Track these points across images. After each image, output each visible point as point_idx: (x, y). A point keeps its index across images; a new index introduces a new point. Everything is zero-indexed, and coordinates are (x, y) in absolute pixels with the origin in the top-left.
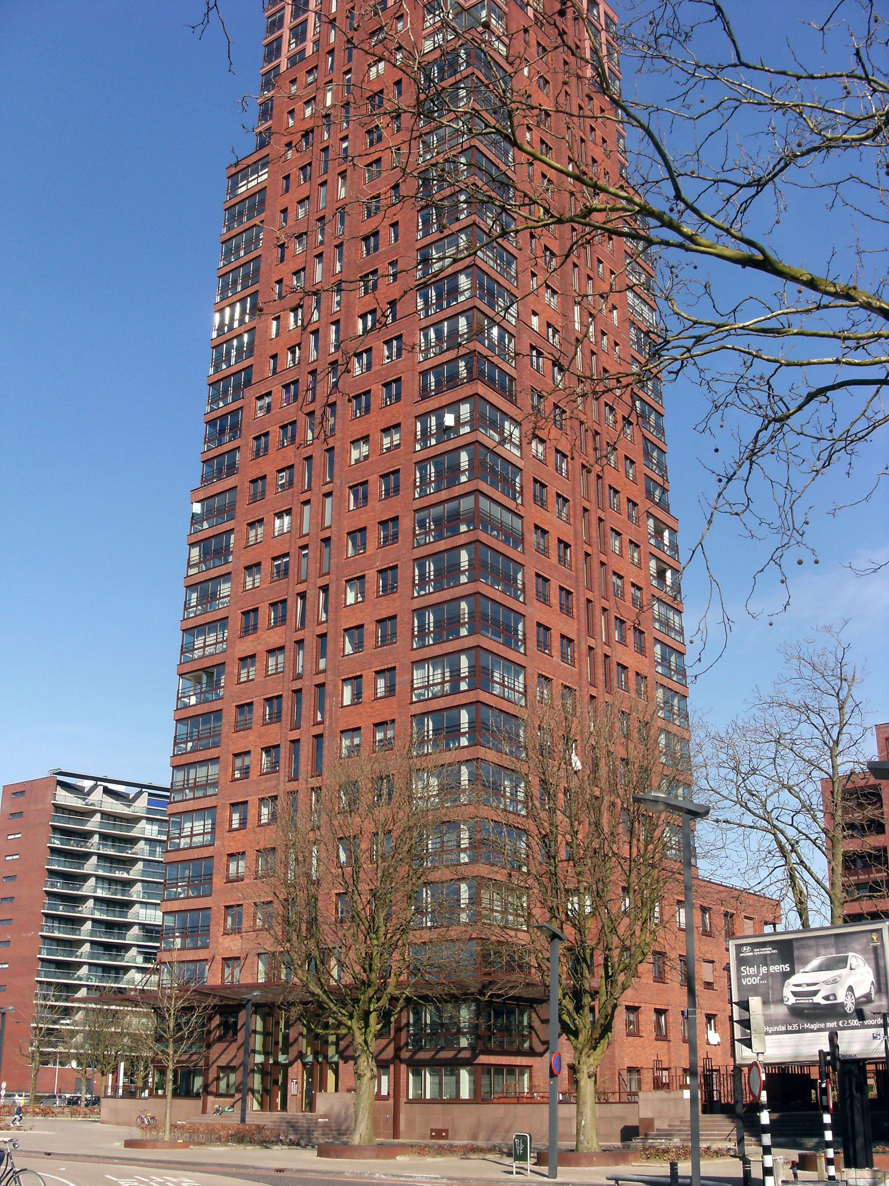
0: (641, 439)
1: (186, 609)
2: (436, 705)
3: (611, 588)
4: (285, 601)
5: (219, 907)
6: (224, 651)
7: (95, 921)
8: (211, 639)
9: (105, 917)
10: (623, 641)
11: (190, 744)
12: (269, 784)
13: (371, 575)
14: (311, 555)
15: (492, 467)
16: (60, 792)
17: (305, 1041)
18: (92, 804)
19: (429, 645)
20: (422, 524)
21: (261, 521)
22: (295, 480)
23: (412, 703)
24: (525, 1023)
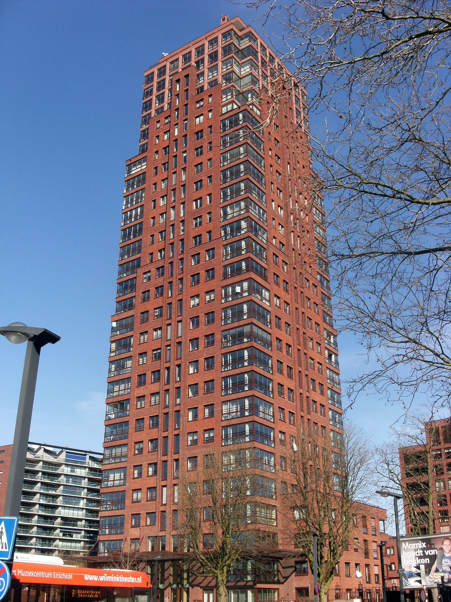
0: (321, 294)
1: (109, 372)
3: (309, 365)
4: (159, 371)
5: (128, 515)
6: (129, 393)
7: (39, 516)
8: (122, 387)
9: (44, 514)
10: (314, 389)
11: (112, 437)
12: (152, 457)
13: (202, 361)
15: (258, 312)
17: (172, 578)
18: (38, 457)
19: (230, 394)
20: (225, 337)
21: (146, 332)
22: (163, 314)
23: (222, 421)
24: (275, 569)
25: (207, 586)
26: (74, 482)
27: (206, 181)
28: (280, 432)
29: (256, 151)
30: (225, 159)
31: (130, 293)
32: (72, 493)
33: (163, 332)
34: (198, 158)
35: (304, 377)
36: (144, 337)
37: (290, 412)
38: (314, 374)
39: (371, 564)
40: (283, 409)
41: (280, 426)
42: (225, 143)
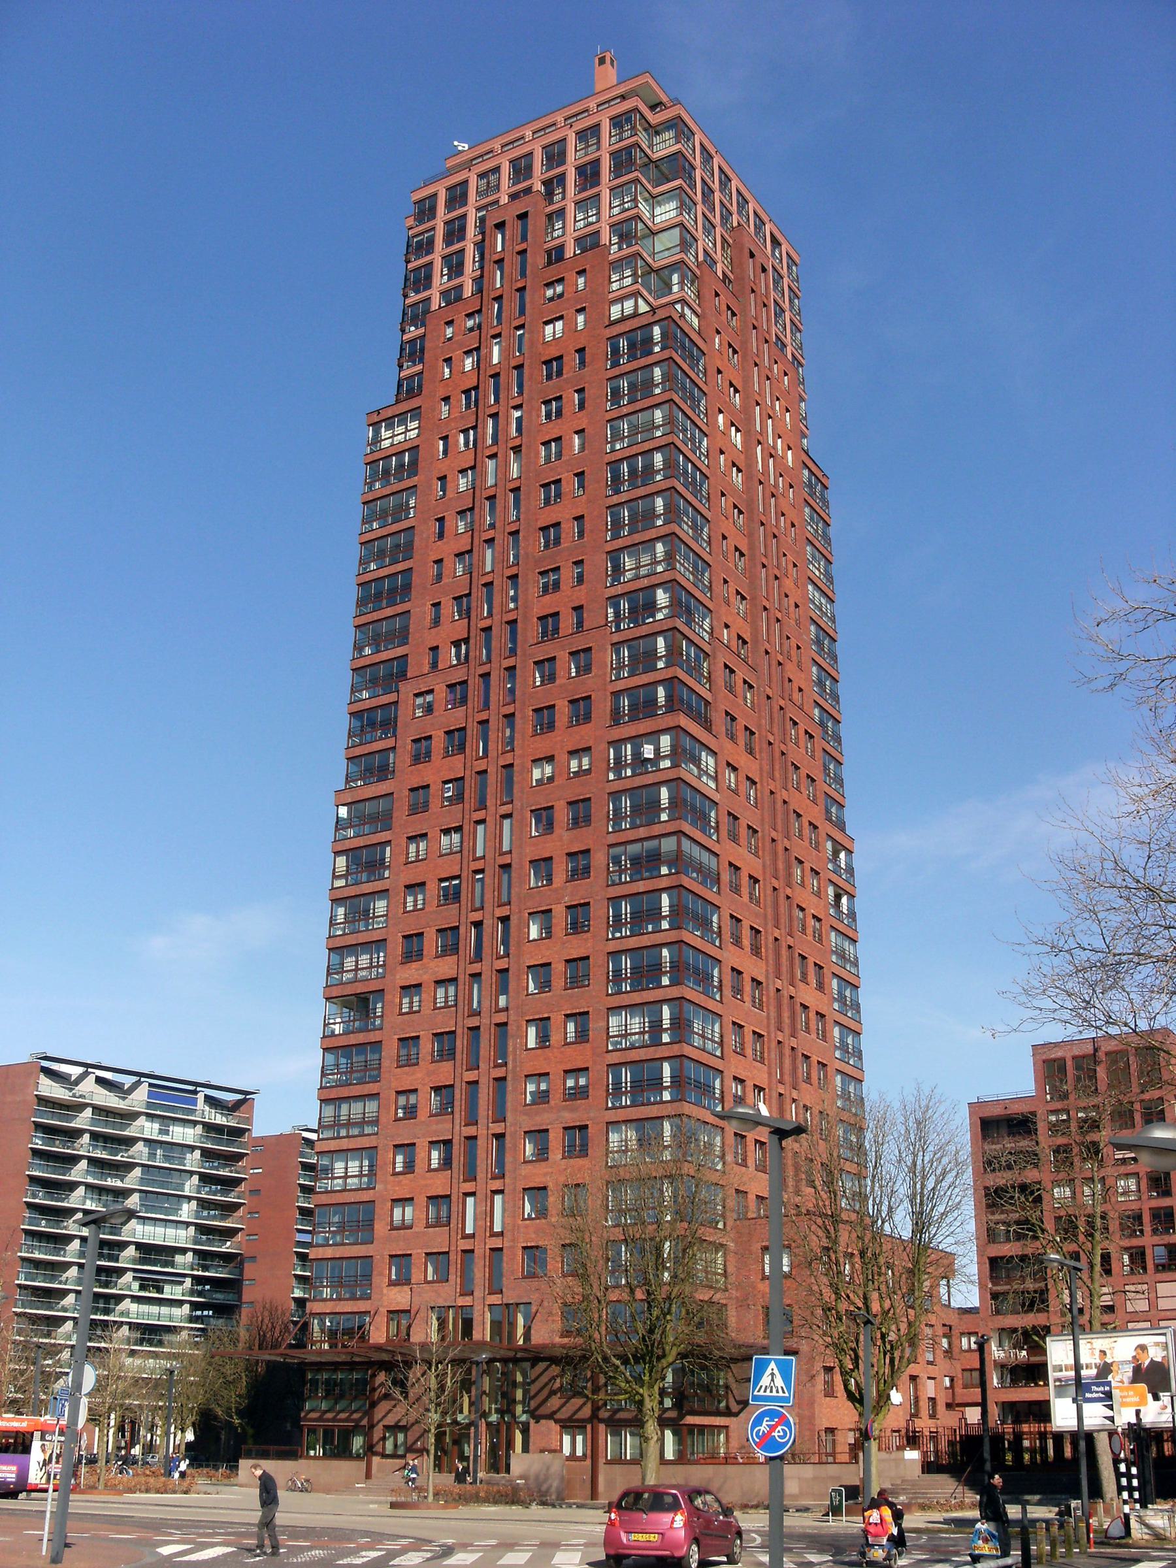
0: (822, 754)
1: (331, 924)
2: (634, 1055)
4: (457, 928)
8: (364, 960)
10: (804, 979)
12: (440, 1126)
13: (559, 911)
14: (488, 881)
15: (690, 804)
16: (44, 1080)
18: (81, 1096)
19: (627, 992)
20: (617, 861)
21: (424, 835)
22: (466, 796)
23: (608, 1051)
25: (570, 1419)
26: (166, 1158)
27: (570, 485)
28: (735, 1078)
29: (689, 418)
30: (617, 436)
31: (381, 739)
32: (163, 1184)
33: (466, 838)
34: (551, 425)
35: (784, 952)
36: (418, 847)
37: (754, 1032)
38: (805, 944)
39: (921, 1375)
40: (741, 1027)
41: (735, 1066)
42: (616, 394)
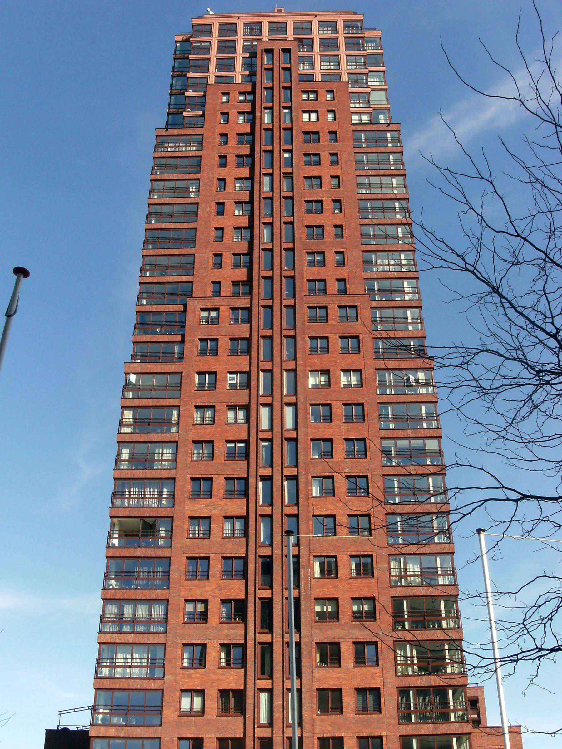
12: (232, 632)
